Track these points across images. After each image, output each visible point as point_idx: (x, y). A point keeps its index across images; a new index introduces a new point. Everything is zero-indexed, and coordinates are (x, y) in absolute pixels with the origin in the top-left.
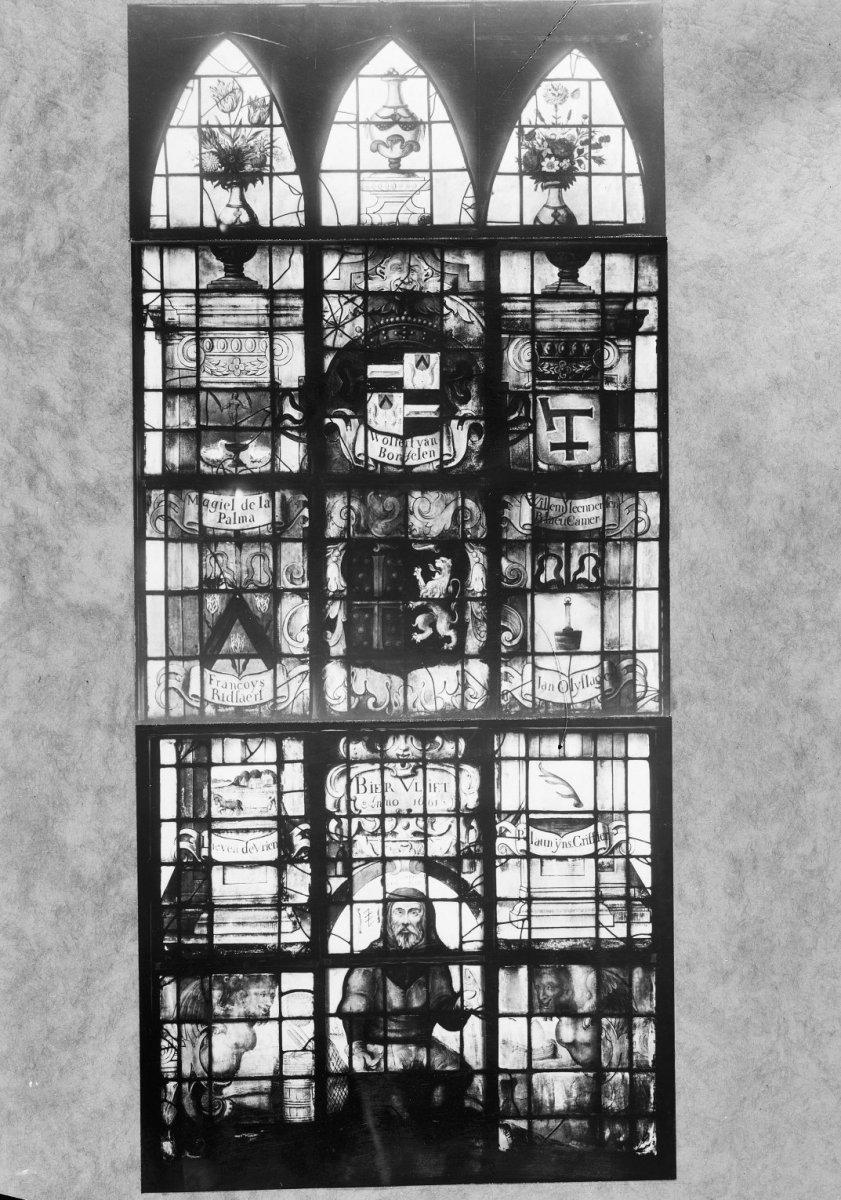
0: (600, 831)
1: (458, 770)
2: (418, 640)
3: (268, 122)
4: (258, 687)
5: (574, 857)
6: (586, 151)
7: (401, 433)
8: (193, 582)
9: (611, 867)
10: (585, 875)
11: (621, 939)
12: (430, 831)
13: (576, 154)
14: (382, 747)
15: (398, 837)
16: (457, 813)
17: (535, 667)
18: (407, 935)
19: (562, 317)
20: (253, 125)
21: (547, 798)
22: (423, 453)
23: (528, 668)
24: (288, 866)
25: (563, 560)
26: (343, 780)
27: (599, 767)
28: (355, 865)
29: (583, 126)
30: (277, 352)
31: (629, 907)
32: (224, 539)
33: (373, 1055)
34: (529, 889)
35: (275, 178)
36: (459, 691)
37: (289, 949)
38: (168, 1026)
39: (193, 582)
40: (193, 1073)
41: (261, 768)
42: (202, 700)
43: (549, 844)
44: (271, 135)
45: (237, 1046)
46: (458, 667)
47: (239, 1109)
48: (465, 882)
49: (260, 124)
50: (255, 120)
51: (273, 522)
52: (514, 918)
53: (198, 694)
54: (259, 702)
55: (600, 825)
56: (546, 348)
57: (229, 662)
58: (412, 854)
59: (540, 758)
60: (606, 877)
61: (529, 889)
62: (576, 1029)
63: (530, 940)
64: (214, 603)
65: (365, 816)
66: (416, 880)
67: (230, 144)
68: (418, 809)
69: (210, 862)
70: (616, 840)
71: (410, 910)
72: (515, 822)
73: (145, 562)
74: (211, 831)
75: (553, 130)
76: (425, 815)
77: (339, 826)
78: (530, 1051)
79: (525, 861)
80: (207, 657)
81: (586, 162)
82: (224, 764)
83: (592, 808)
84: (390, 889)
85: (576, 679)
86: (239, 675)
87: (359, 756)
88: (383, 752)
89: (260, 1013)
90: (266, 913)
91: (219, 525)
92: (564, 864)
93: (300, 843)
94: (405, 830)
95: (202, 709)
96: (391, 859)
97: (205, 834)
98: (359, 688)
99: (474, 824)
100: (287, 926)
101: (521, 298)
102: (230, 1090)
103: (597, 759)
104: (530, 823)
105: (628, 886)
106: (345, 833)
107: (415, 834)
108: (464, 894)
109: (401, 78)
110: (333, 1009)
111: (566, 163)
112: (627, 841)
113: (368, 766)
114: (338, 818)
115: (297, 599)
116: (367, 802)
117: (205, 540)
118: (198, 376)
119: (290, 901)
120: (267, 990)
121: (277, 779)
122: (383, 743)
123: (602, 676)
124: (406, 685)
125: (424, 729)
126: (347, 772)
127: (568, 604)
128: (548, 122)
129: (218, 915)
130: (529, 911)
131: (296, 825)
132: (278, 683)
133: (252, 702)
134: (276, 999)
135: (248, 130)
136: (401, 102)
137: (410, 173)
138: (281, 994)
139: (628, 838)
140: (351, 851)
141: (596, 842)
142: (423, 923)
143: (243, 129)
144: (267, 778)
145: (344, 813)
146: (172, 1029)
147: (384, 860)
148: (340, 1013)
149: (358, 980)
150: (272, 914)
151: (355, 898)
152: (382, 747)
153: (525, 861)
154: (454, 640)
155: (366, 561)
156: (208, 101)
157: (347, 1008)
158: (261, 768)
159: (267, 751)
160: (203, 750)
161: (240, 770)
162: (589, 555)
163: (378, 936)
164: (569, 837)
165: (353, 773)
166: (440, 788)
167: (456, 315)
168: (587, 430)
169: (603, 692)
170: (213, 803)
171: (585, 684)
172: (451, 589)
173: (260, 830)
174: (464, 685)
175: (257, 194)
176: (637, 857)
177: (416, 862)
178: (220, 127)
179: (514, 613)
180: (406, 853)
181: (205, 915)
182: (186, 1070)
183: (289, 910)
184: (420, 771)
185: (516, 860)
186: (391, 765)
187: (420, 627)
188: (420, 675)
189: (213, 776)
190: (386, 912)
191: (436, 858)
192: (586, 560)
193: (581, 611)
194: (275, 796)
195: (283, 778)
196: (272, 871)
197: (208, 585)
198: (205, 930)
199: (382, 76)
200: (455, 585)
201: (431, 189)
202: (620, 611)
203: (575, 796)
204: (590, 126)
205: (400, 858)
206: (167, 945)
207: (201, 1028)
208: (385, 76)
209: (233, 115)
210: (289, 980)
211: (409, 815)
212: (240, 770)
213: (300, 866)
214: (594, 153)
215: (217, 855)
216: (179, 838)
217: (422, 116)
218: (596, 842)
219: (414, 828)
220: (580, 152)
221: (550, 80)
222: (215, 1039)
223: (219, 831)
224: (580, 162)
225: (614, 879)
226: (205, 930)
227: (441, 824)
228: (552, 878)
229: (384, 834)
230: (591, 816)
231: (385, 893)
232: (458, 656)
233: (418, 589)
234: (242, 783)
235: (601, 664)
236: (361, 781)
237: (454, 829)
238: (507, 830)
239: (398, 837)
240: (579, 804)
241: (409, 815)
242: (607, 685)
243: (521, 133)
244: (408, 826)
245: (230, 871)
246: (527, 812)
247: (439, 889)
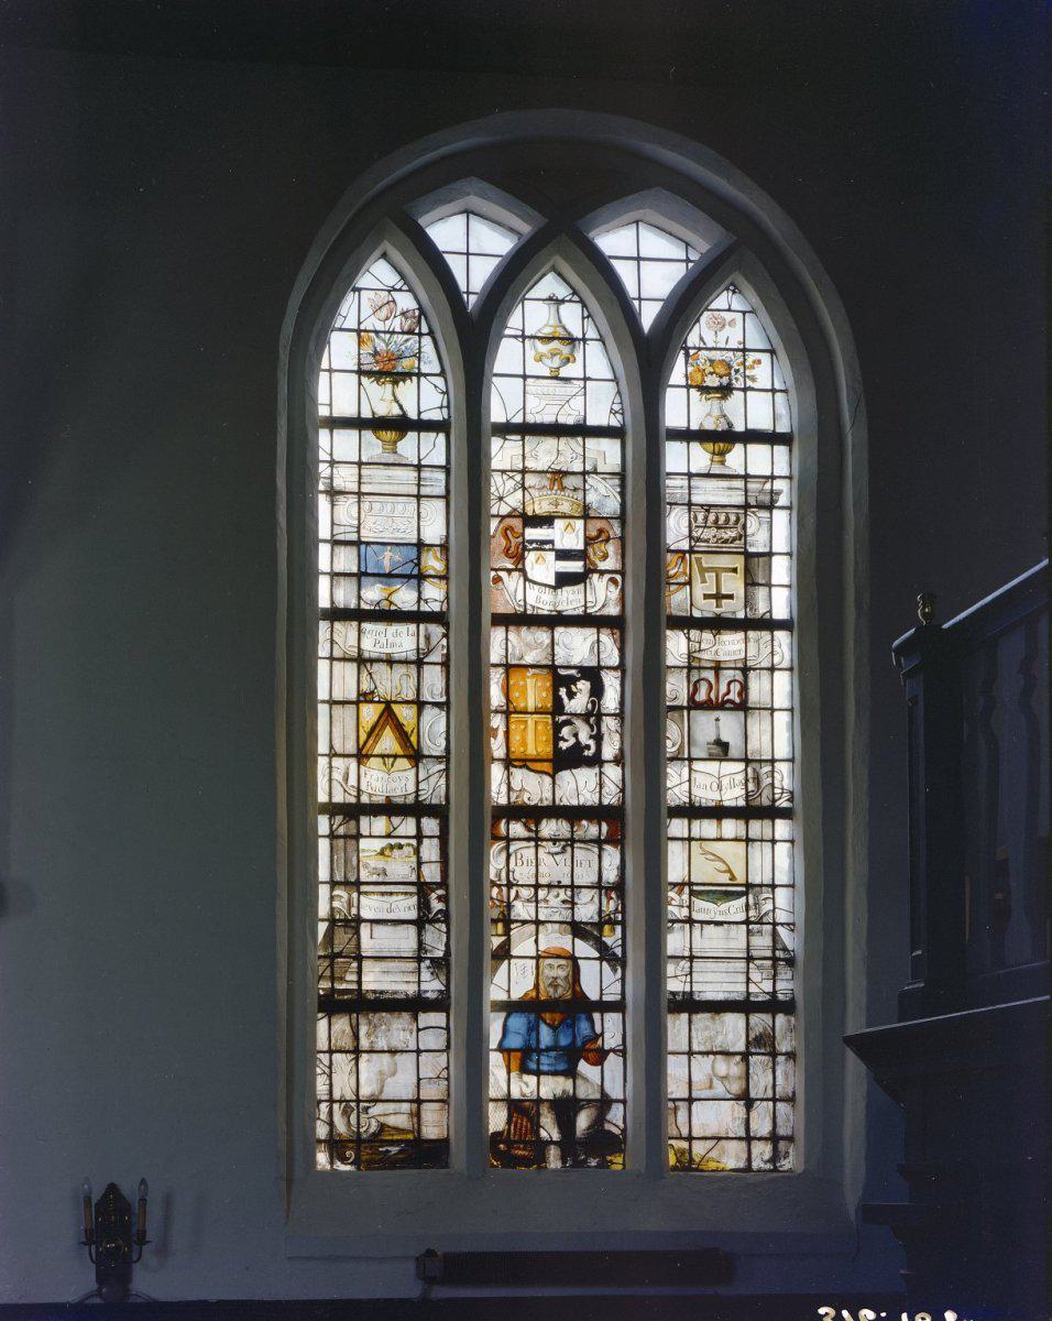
0: (751, 901)
1: (601, 850)
2: (564, 748)
3: (417, 331)
4: (404, 782)
5: (729, 923)
6: (742, 371)
7: (553, 583)
8: (353, 696)
9: (760, 932)
10: (737, 940)
11: (767, 993)
12: (576, 900)
14: (537, 826)
16: (599, 886)
18: (556, 987)
19: (708, 492)
20: (403, 333)
21: (706, 872)
22: (571, 600)
23: (686, 769)
24: (427, 926)
25: (713, 682)
26: (504, 855)
27: (749, 848)
28: (512, 926)
29: (738, 350)
30: (422, 515)
31: (774, 967)
32: (378, 660)
34: (691, 949)
35: (422, 379)
36: (598, 790)
38: (321, 1056)
41: (403, 842)
44: (420, 342)
46: (597, 770)
49: (410, 332)
50: (406, 328)
52: (679, 973)
53: (355, 785)
54: (404, 793)
55: (751, 896)
57: (380, 760)
59: (701, 839)
60: (756, 941)
61: (691, 949)
62: (729, 1064)
64: (370, 713)
65: (522, 886)
66: (564, 942)
67: (385, 348)
68: (567, 881)
69: (358, 920)
71: (559, 966)
72: (680, 893)
73: (316, 679)
75: (714, 352)
76: (572, 887)
80: (361, 756)
81: (742, 379)
83: (744, 882)
84: (542, 947)
85: (725, 781)
86: (389, 770)
88: (537, 832)
90: (408, 964)
92: (720, 928)
93: (436, 906)
94: (555, 899)
95: (358, 797)
96: (543, 922)
97: (355, 895)
98: (516, 785)
99: (613, 895)
100: (426, 975)
104: (692, 893)
105: (774, 949)
106: (505, 900)
107: (564, 902)
108: (605, 954)
110: (493, 1044)
111: (725, 381)
113: (525, 844)
114: (499, 886)
116: (523, 874)
117: (361, 661)
118: (358, 532)
119: (429, 955)
121: (417, 851)
122: (537, 824)
124: (554, 783)
125: (574, 814)
126: (507, 848)
128: (709, 346)
130: (691, 967)
132: (421, 778)
134: (415, 1033)
135: (400, 336)
136: (560, 322)
138: (419, 1030)
140: (509, 914)
141: (747, 910)
142: (570, 978)
143: (396, 336)
144: (408, 850)
146: (324, 1058)
147: (538, 923)
152: (537, 826)
155: (521, 683)
156: (366, 311)
158: (403, 842)
159: (407, 826)
162: (735, 681)
164: (724, 906)
165: (512, 849)
167: (596, 490)
168: (734, 585)
169: (747, 792)
171: (733, 785)
172: (590, 706)
173: (402, 893)
176: (782, 924)
177: (564, 926)
178: (376, 332)
179: (673, 725)
180: (557, 918)
183: (428, 962)
184: (569, 849)
185: (680, 925)
186: (544, 843)
187: (566, 737)
188: (565, 776)
189: (361, 847)
191: (581, 923)
192: (732, 686)
194: (415, 865)
195: (421, 850)
196: (412, 930)
197: (365, 697)
198: (354, 977)
199: (544, 300)
200: (593, 703)
201: (585, 395)
202: (758, 726)
203: (730, 871)
205: (551, 922)
206: (323, 989)
207: (350, 1058)
208: (546, 300)
211: (559, 886)
213: (437, 925)
214: (748, 373)
215: (365, 914)
216: (332, 898)
217: (578, 334)
218: (747, 910)
220: (737, 371)
221: (711, 310)
223: (366, 893)
224: (737, 379)
225: (762, 943)
229: (537, 902)
230: (744, 889)
231: (538, 950)
232: (596, 761)
233: (563, 707)
234: (387, 852)
235: (746, 770)
236: (519, 857)
237: (596, 899)
238: (672, 899)
240: (733, 878)
241: (559, 886)
242: (751, 786)
243: (687, 355)
244: (558, 895)
246: (690, 884)
247: (584, 949)
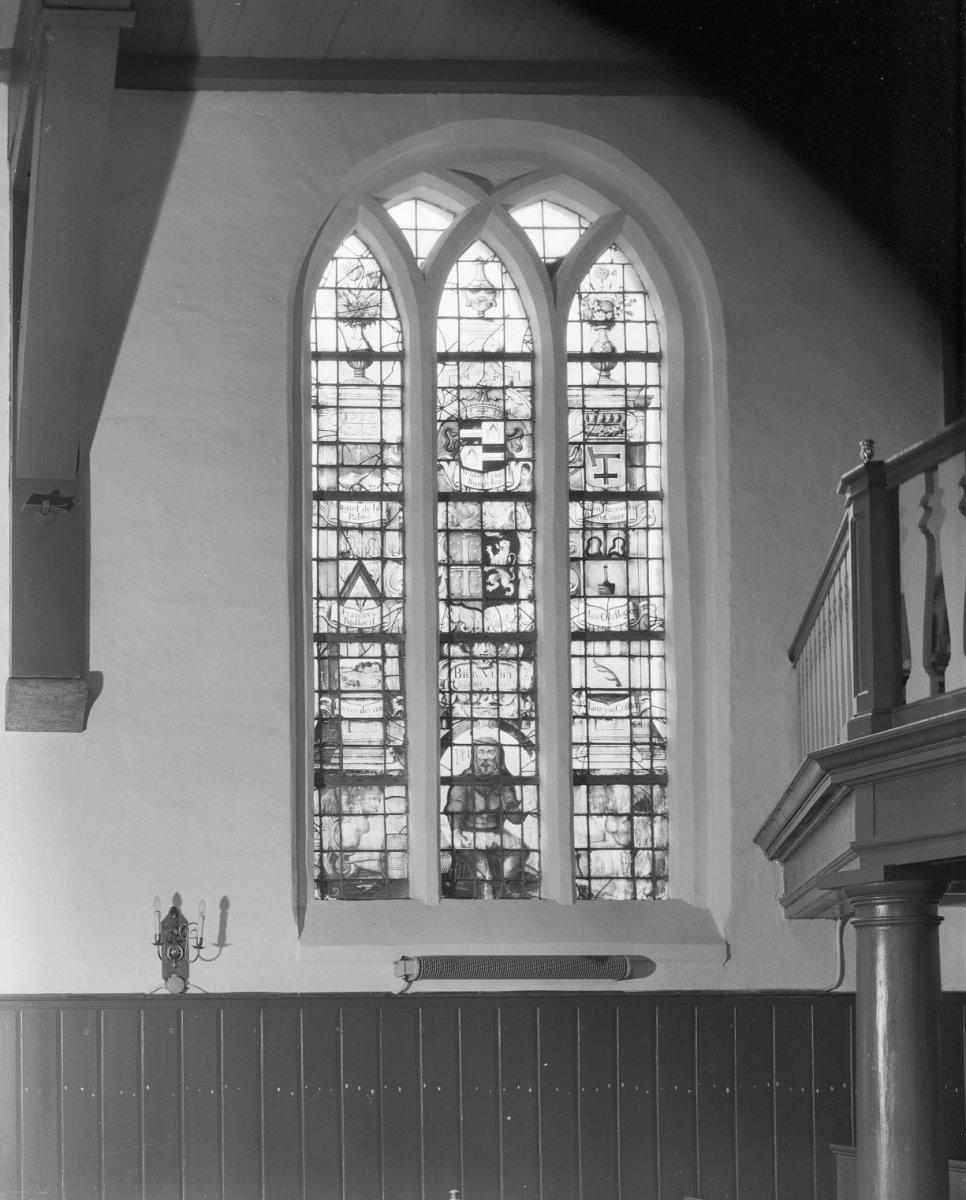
1: (519, 665)
7: (481, 469)
8: (334, 555)
12: (501, 702)
13: (615, 309)
15: (482, 705)
17: (586, 604)
18: (486, 766)
20: (369, 289)
21: (598, 680)
23: (582, 605)
26: (446, 670)
28: (454, 722)
31: (651, 750)
33: (466, 838)
37: (391, 773)
39: (334, 555)
40: (330, 847)
41: (372, 661)
42: (339, 624)
43: (600, 709)
45: (358, 830)
46: (515, 606)
47: (360, 870)
48: (523, 734)
49: (374, 288)
51: (382, 520)
55: (633, 698)
56: (592, 417)
58: (490, 716)
60: (637, 731)
63: (588, 770)
65: (460, 692)
69: (340, 718)
70: (643, 707)
72: (579, 696)
74: (341, 699)
77: (444, 697)
78: (589, 837)
79: (585, 720)
81: (622, 314)
82: (348, 657)
83: (627, 687)
84: (476, 738)
85: (612, 613)
87: (456, 655)
88: (471, 652)
89: (372, 811)
90: (377, 751)
91: (348, 520)
94: (485, 702)
95: (338, 629)
96: (477, 719)
97: (337, 700)
98: (455, 618)
99: (529, 698)
100: (390, 759)
101: (952, 760)
102: (355, 857)
103: (631, 657)
104: (588, 696)
107: (492, 704)
109: (485, 262)
112: (650, 709)
113: (462, 661)
114: (443, 693)
115: (396, 564)
118: (337, 435)
119: (392, 744)
120: (375, 796)
121: (382, 668)
122: (472, 646)
123: (629, 612)
124: (483, 616)
125: (498, 639)
126: (449, 664)
127: (606, 567)
128: (597, 290)
129: (346, 751)
131: (394, 697)
133: (368, 625)
135: (367, 292)
137: (491, 319)
138: (385, 799)
139: (651, 706)
144: (375, 667)
145: (447, 690)
147: (473, 719)
148: (446, 812)
149: (457, 791)
150: (380, 752)
151: (455, 741)
153: (585, 720)
154: (512, 590)
157: (450, 809)
158: (372, 661)
159: (375, 650)
160: (335, 648)
161: (358, 662)
163: (468, 766)
164: (613, 705)
165: (453, 665)
166: (507, 675)
168: (618, 466)
169: (629, 621)
170: (341, 681)
171: (618, 615)
172: (510, 559)
174: (519, 617)
175: (372, 331)
176: (657, 718)
178: (349, 289)
181: (337, 751)
182: (326, 846)
183: (391, 749)
184: (495, 665)
186: (476, 661)
188: (491, 611)
190: (473, 752)
192: (617, 541)
193: (614, 571)
200: (512, 556)
202: (637, 570)
203: (616, 679)
204: (624, 293)
209: (358, 282)
210: (390, 791)
211: (488, 692)
212: (358, 662)
214: (627, 309)
215: (345, 714)
216: (320, 703)
217: (498, 285)
219: (491, 700)
222: (343, 825)
223: (345, 699)
225: (642, 732)
226: (337, 761)
227: (508, 699)
228: (601, 731)
230: (627, 692)
232: (515, 599)
233: (489, 560)
234: (360, 669)
235: (628, 604)
237: (516, 702)
239: (482, 705)
240: (619, 684)
241: (488, 692)
242: (632, 616)
245: (353, 724)
247: (507, 738)
